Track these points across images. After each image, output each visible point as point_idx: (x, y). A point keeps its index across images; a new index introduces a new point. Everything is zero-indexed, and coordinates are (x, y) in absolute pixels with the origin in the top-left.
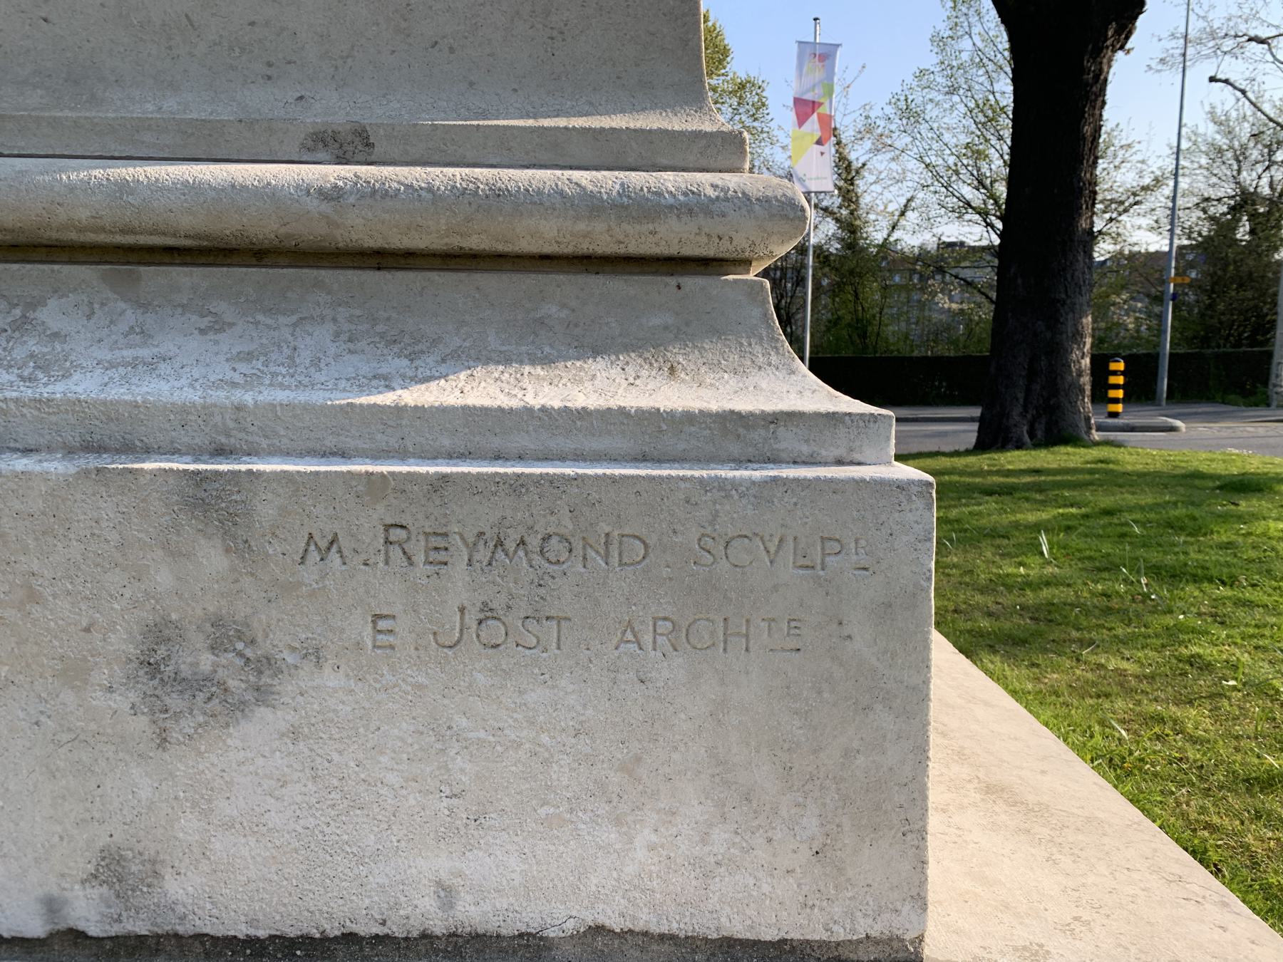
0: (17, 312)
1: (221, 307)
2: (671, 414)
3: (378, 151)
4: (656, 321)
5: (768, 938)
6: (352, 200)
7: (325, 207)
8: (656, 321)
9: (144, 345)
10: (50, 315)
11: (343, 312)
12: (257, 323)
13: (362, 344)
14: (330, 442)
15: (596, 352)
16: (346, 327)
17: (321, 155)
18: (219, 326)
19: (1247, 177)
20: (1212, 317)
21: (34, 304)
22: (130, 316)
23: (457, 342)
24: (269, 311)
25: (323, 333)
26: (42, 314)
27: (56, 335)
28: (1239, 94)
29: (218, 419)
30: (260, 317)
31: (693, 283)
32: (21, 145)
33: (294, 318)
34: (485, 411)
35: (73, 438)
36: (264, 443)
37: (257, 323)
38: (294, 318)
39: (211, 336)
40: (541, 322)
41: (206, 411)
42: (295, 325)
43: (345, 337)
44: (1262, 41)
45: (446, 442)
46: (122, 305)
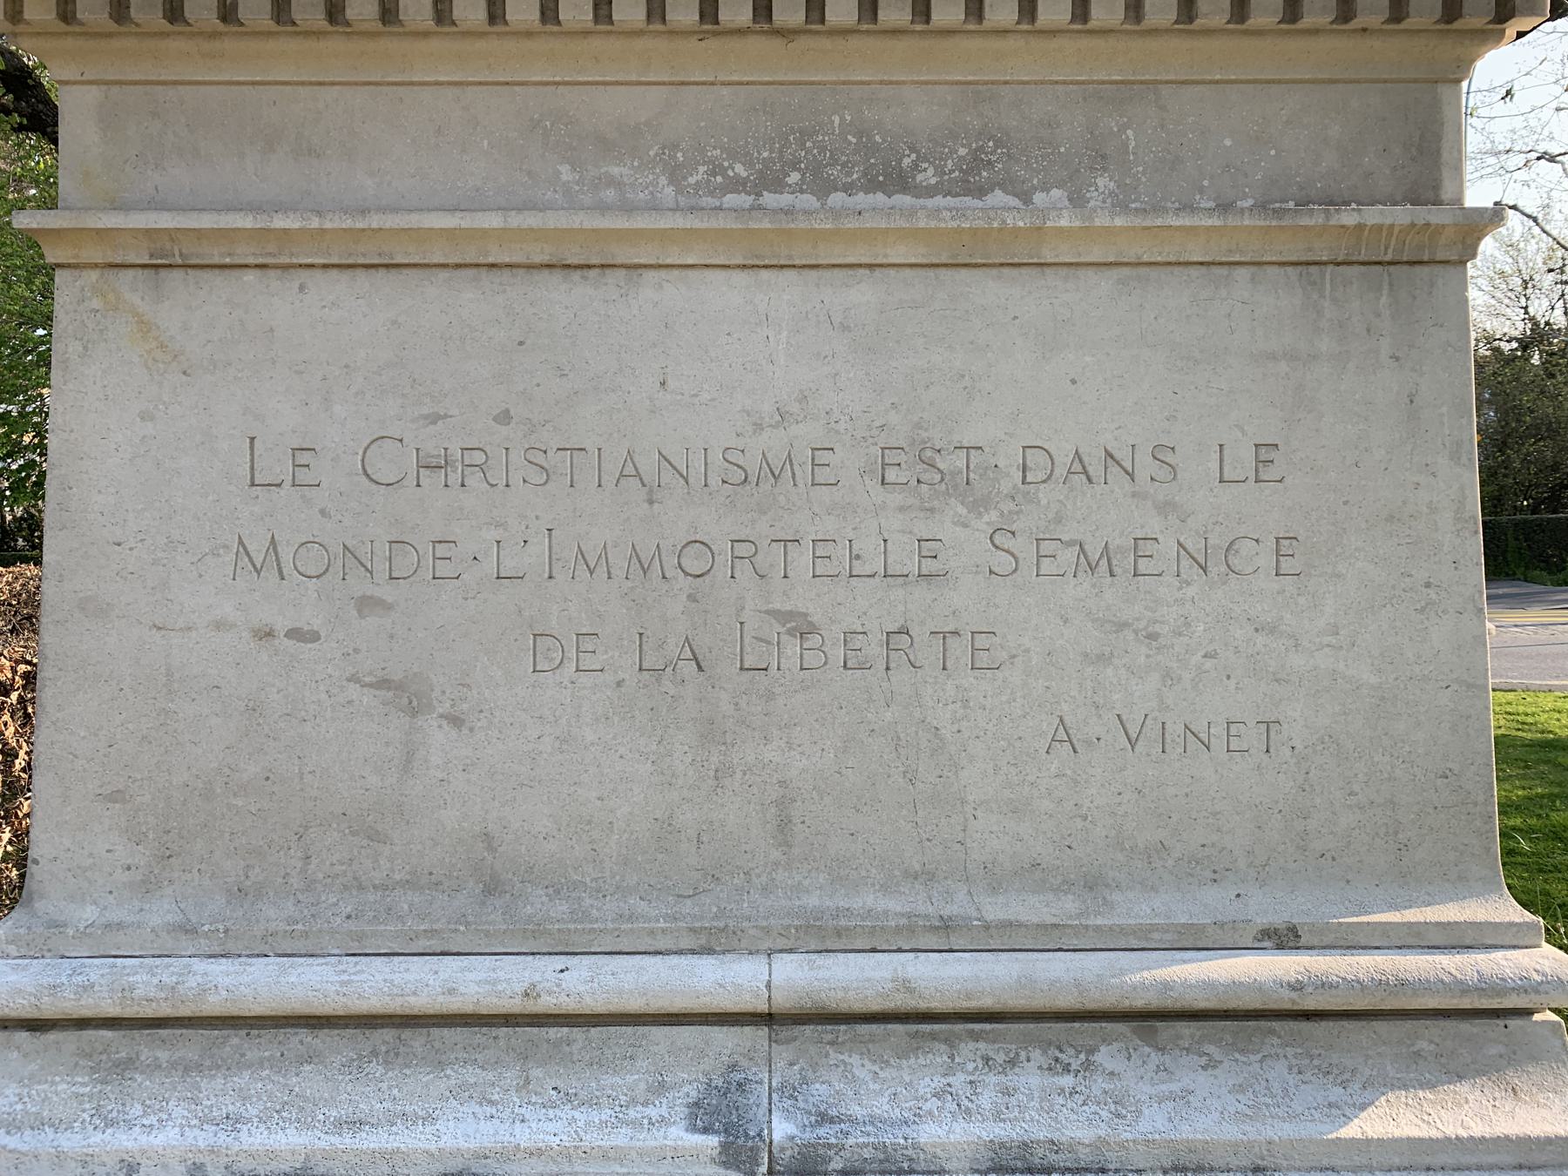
0: (1082, 1056)
1: (1210, 1048)
2: (1538, 1139)
3: (1303, 941)
4: (1493, 1051)
5: (385, 1031)
6: (1310, 990)
7: (1294, 995)
8: (1493, 1051)
9: (1171, 1081)
10: (1105, 1057)
11: (1290, 1051)
12: (1236, 1060)
13: (1308, 1076)
14: (1325, 1162)
15: (1461, 1077)
16: (1294, 1062)
17: (1266, 944)
18: (1211, 1065)
19: (1538, 308)
20: (1505, 476)
21: (1092, 1051)
22: (1155, 1058)
23: (1367, 1072)
24: (1241, 1051)
25: (1281, 1067)
26: (1098, 1058)
27: (1112, 1073)
28: (1532, 223)
29: (1257, 1149)
30: (1237, 1055)
31: (1514, 1023)
32: (1076, 943)
33: (1259, 1056)
34: (1421, 1140)
35: (1167, 1164)
36: (1285, 1163)
37: (1236, 1060)
38: (1259, 1056)
39: (1210, 1071)
40: (1418, 1054)
41: (1250, 1145)
42: (1261, 1061)
43: (1295, 1070)
44: (1552, 159)
45: (1397, 1161)
46: (1147, 1049)
